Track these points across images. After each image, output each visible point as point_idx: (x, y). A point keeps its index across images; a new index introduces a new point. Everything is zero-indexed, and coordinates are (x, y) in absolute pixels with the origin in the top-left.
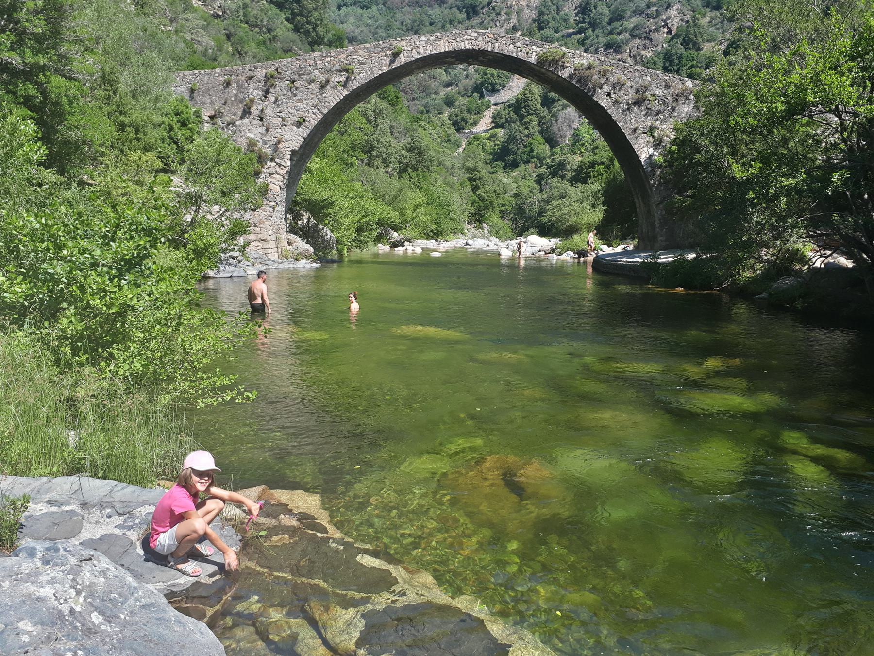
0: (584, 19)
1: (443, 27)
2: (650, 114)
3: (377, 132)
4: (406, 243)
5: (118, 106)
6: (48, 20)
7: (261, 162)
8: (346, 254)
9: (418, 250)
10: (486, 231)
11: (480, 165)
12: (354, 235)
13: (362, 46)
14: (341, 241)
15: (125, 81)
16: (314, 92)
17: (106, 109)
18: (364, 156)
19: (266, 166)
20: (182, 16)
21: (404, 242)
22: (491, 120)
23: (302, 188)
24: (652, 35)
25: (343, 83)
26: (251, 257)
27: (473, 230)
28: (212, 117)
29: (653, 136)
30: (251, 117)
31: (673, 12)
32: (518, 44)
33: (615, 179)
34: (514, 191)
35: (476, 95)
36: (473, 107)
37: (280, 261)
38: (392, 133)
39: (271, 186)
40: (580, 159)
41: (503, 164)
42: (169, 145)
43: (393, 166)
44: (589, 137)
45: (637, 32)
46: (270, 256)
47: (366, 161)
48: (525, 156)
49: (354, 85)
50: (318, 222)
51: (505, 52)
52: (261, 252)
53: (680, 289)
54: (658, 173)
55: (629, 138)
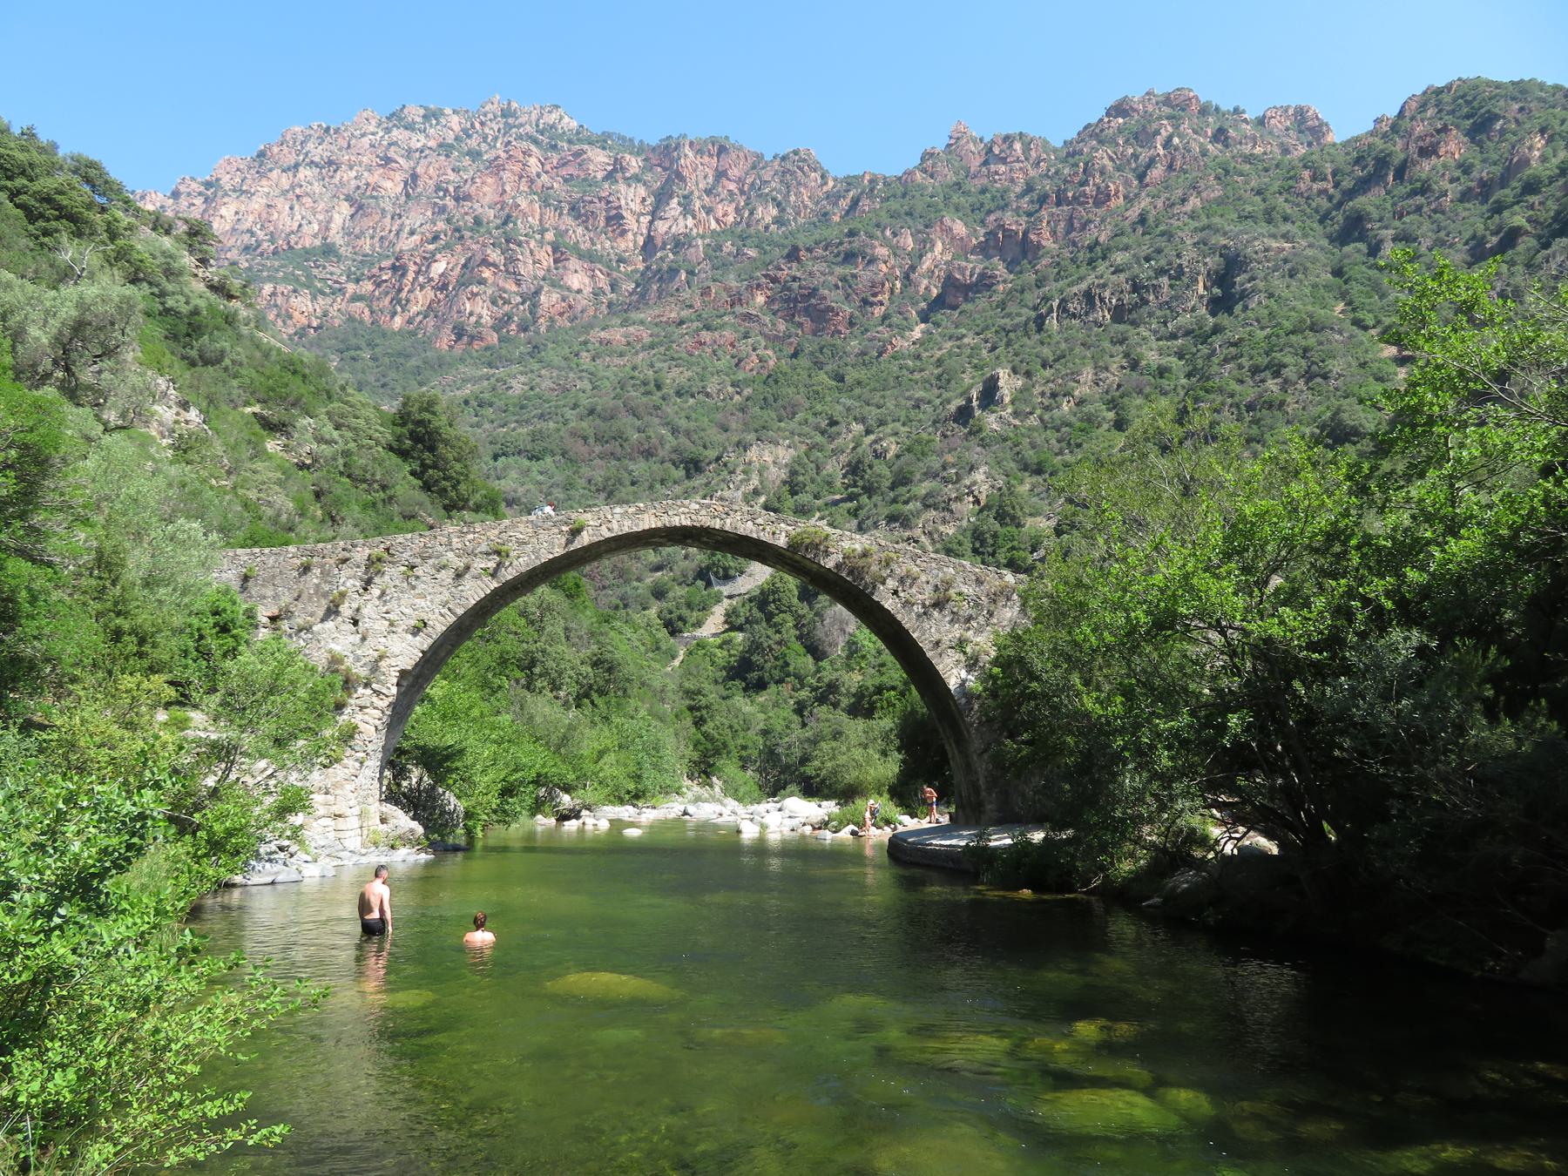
0: (855, 482)
1: (651, 487)
2: (958, 621)
3: (543, 639)
4: (584, 812)
5: (116, 604)
6: (21, 479)
7: (348, 689)
8: (480, 835)
9: (604, 825)
10: (717, 789)
11: (707, 687)
12: (495, 802)
13: (524, 519)
14: (473, 814)
15: (136, 563)
16: (445, 583)
17: (95, 606)
18: (518, 674)
19: (355, 696)
20: (249, 465)
21: (580, 811)
22: (723, 619)
23: (413, 727)
24: (953, 506)
25: (491, 571)
26: (313, 844)
27: (696, 789)
28: (273, 619)
29: (965, 653)
30: (340, 619)
31: (979, 476)
32: (760, 521)
33: (914, 712)
34: (761, 726)
35: (700, 583)
36: (697, 600)
37: (363, 851)
38: (568, 638)
39: (362, 727)
40: (860, 678)
41: (744, 684)
42: (195, 661)
43: (568, 690)
44: (871, 645)
45: (931, 501)
46: (347, 843)
47: (523, 681)
48: (777, 674)
49: (508, 574)
50: (436, 782)
51: (741, 532)
52: (332, 835)
53: (1026, 893)
54: (976, 707)
55: (929, 654)
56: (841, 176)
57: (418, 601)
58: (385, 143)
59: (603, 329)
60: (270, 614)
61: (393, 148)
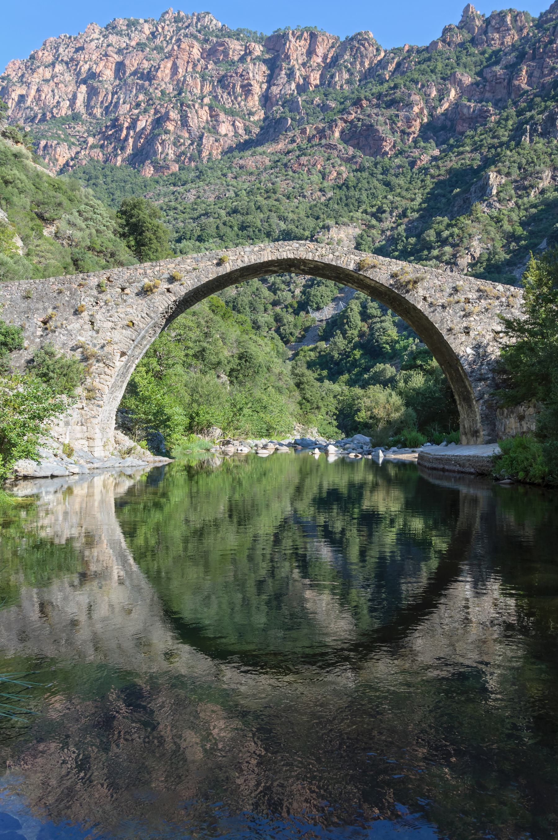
55: (446, 337)
56: (389, 48)
57: (128, 309)
58: (105, 45)
59: (241, 158)
60: (42, 319)
61: (110, 48)
